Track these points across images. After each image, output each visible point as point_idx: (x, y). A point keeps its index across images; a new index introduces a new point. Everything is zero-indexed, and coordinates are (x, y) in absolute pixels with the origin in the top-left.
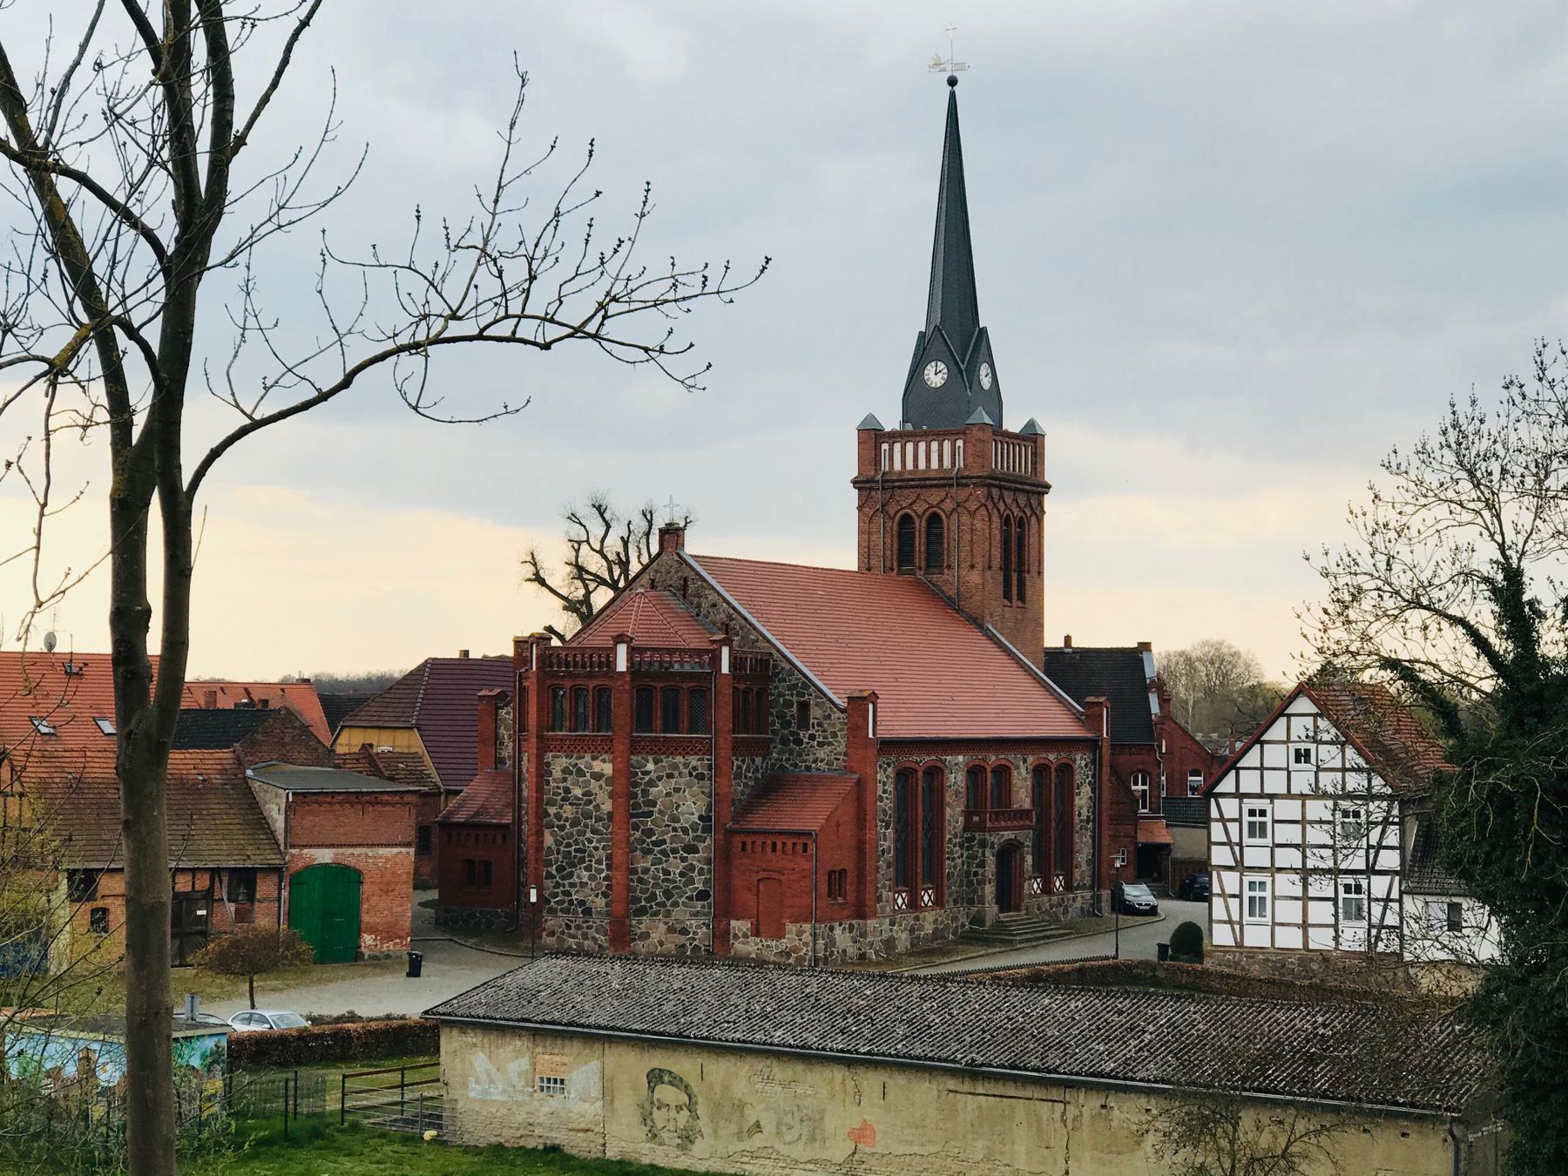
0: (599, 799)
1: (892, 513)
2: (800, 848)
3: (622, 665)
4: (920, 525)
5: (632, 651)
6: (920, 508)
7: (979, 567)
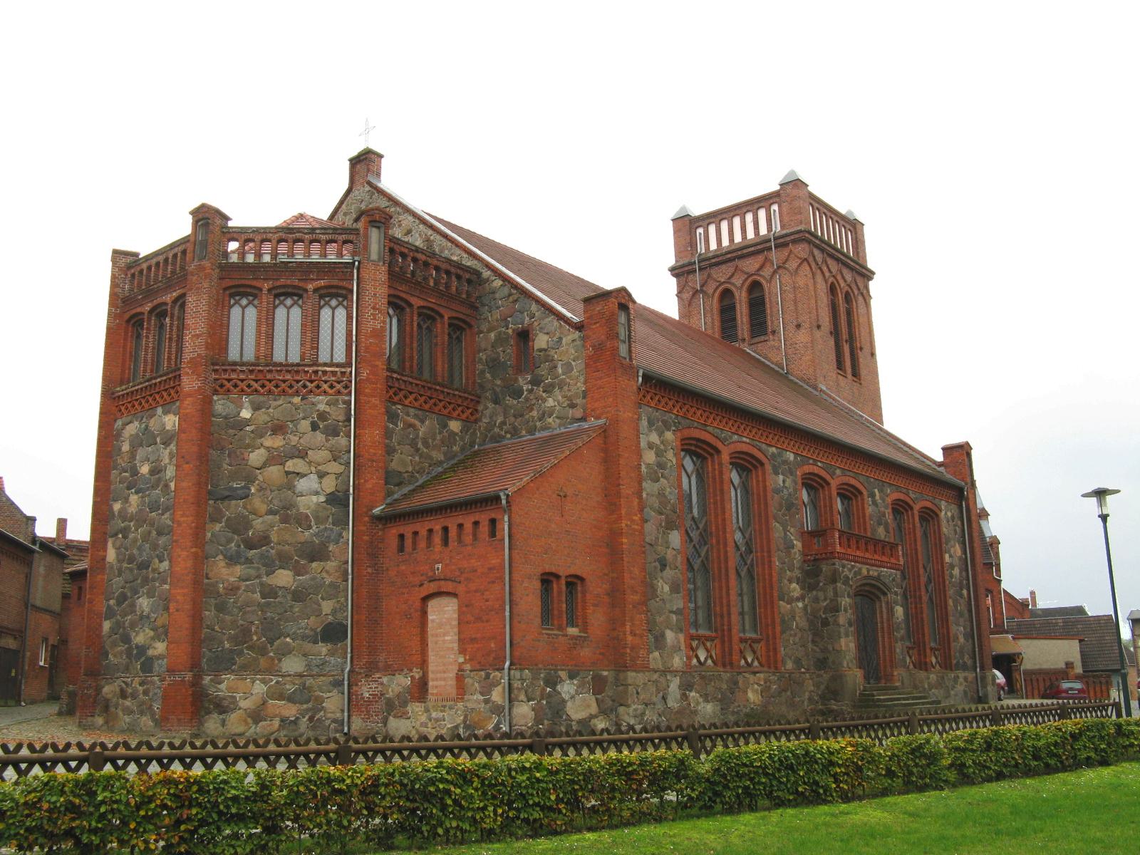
1: (710, 291)
2: (484, 529)
4: (741, 298)
7: (807, 325)
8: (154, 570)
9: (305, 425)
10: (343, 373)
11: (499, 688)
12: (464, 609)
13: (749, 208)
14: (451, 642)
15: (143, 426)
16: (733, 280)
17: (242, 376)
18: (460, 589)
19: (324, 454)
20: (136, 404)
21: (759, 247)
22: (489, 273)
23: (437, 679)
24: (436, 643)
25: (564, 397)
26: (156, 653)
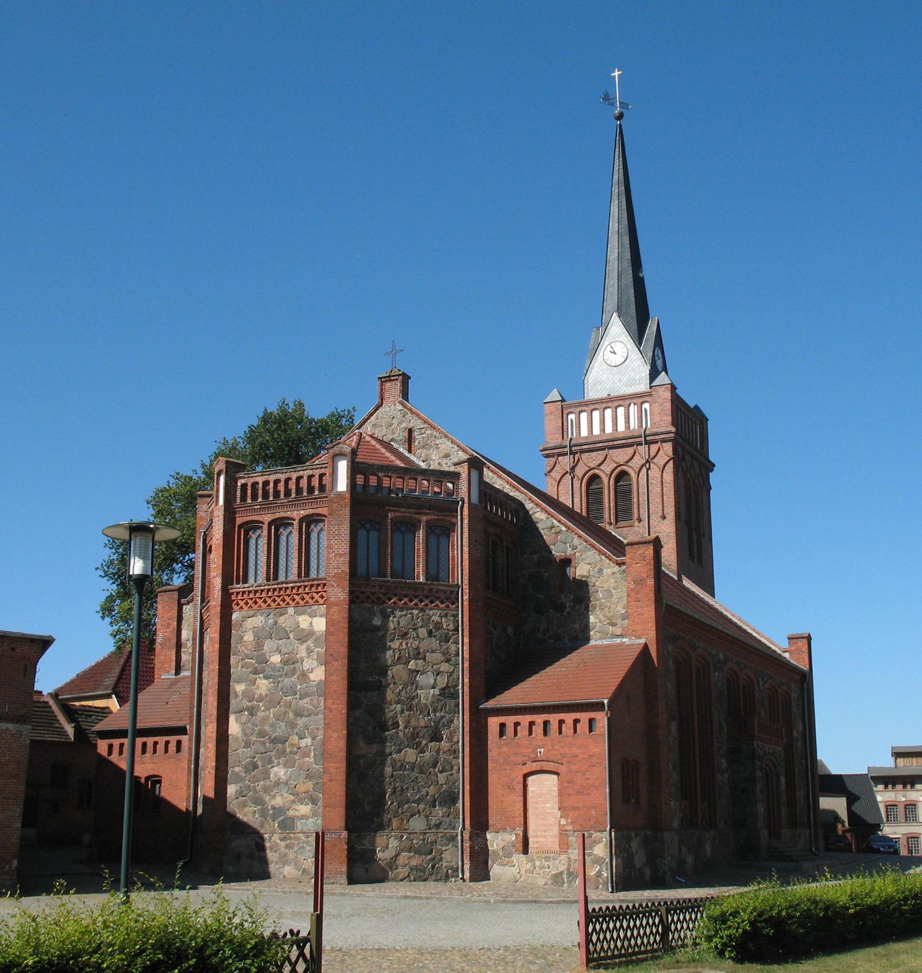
0: (306, 666)
3: (342, 485)
5: (355, 469)
6: (608, 467)
8: (292, 745)
9: (423, 632)
10: (452, 592)
11: (601, 845)
12: (566, 784)
13: (620, 402)
14: (552, 808)
15: (271, 621)
16: (602, 467)
17: (373, 590)
18: (561, 769)
19: (438, 656)
20: (260, 602)
21: (630, 441)
22: (532, 505)
23: (537, 836)
24: (537, 808)
25: (604, 616)
26: (297, 814)
